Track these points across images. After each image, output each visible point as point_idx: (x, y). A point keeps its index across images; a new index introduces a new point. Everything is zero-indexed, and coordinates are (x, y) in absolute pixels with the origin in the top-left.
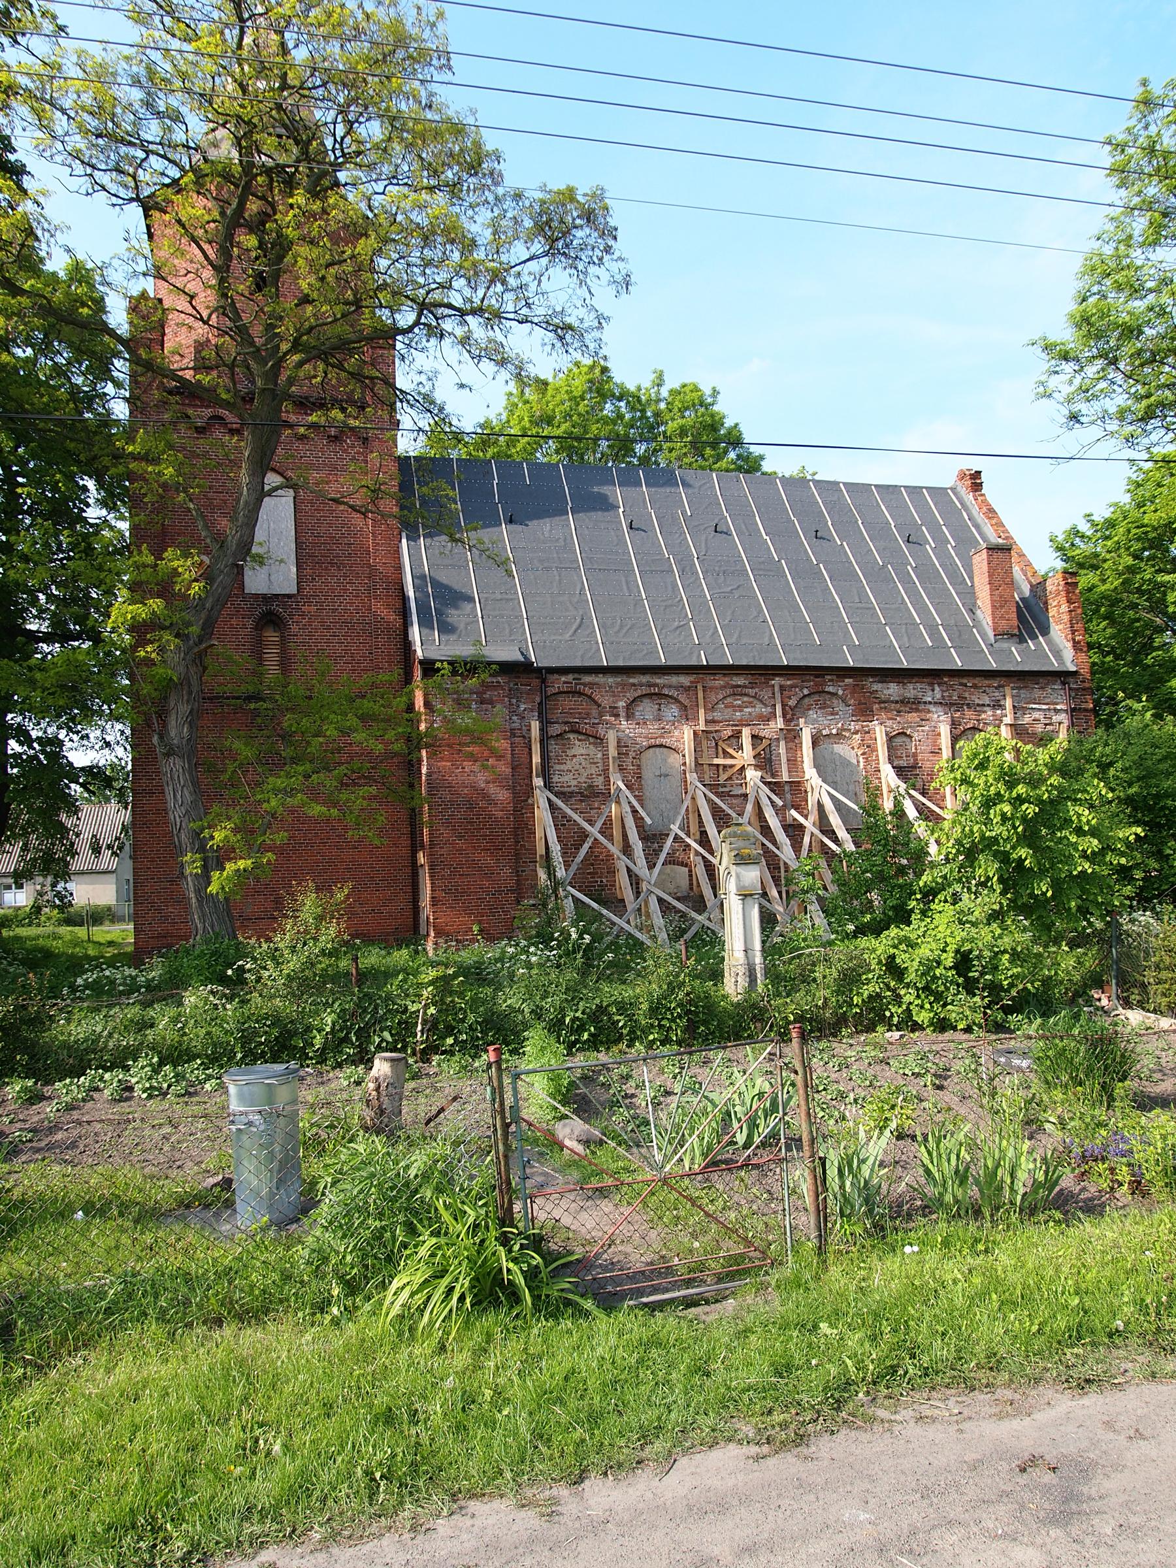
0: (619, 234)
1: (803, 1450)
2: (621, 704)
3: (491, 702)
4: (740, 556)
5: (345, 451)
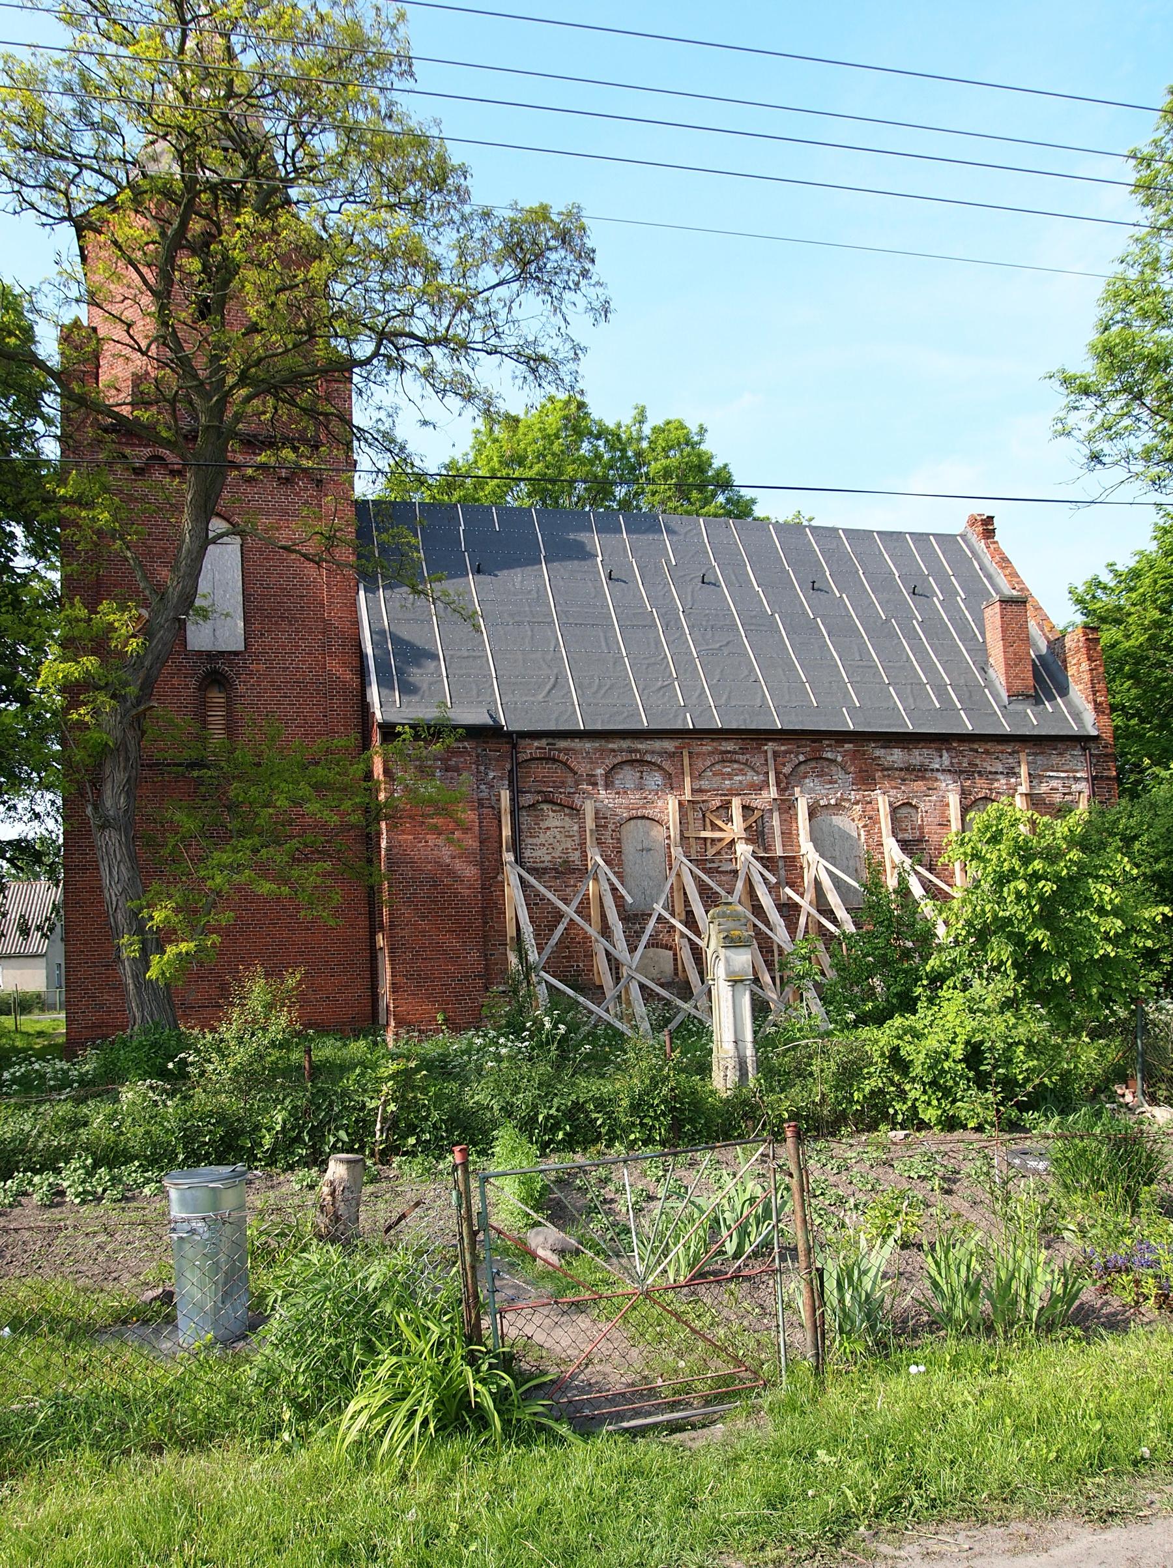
3: (457, 770)
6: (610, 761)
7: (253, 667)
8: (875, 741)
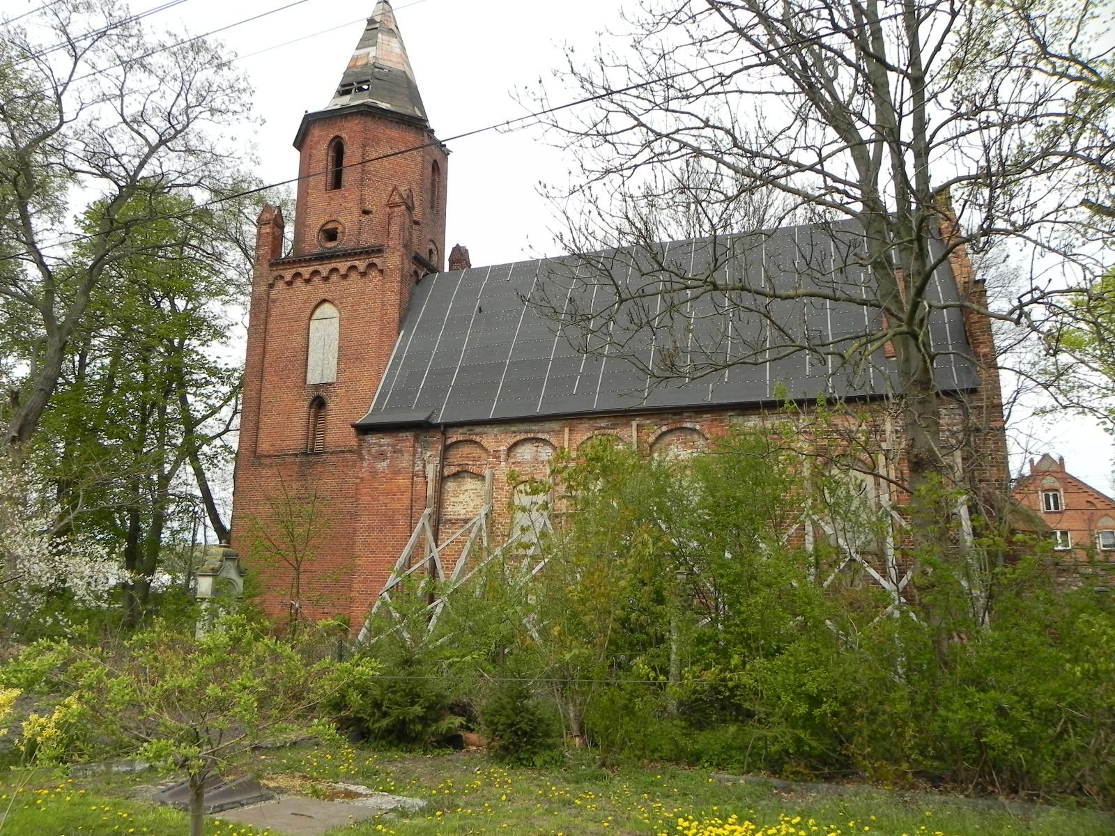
0: (253, 82)
1: (1046, 530)
2: (503, 448)
3: (401, 452)
4: (388, 356)
5: (371, 281)
6: (511, 441)
7: (339, 391)
8: (732, 410)
